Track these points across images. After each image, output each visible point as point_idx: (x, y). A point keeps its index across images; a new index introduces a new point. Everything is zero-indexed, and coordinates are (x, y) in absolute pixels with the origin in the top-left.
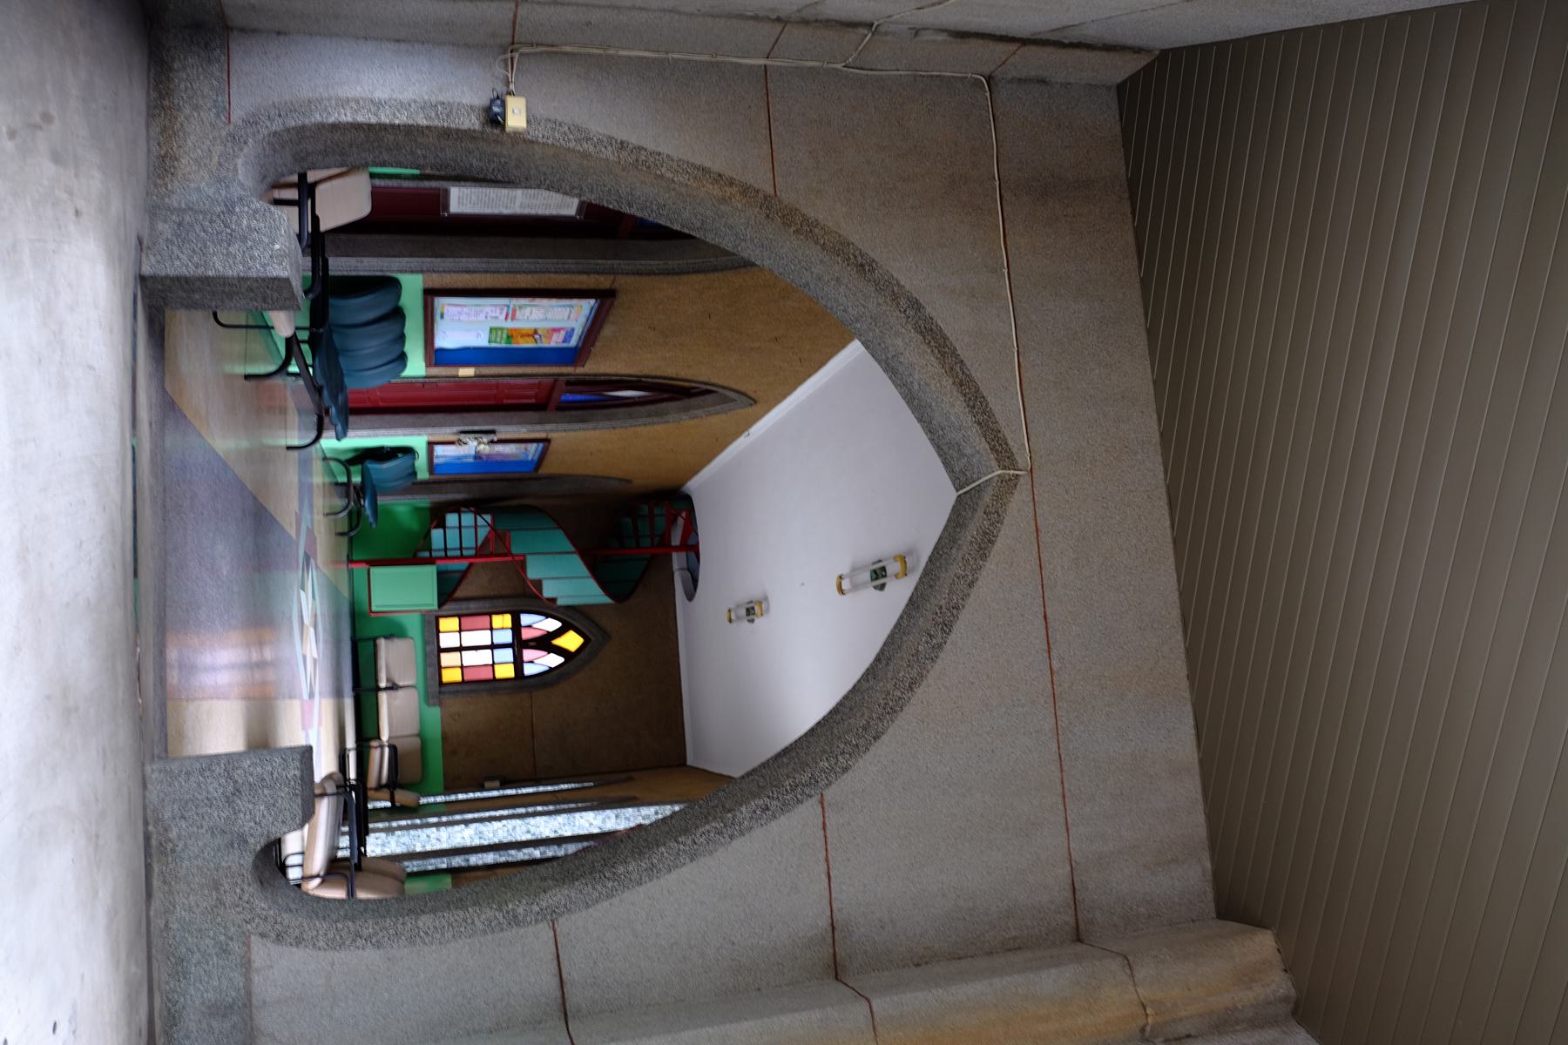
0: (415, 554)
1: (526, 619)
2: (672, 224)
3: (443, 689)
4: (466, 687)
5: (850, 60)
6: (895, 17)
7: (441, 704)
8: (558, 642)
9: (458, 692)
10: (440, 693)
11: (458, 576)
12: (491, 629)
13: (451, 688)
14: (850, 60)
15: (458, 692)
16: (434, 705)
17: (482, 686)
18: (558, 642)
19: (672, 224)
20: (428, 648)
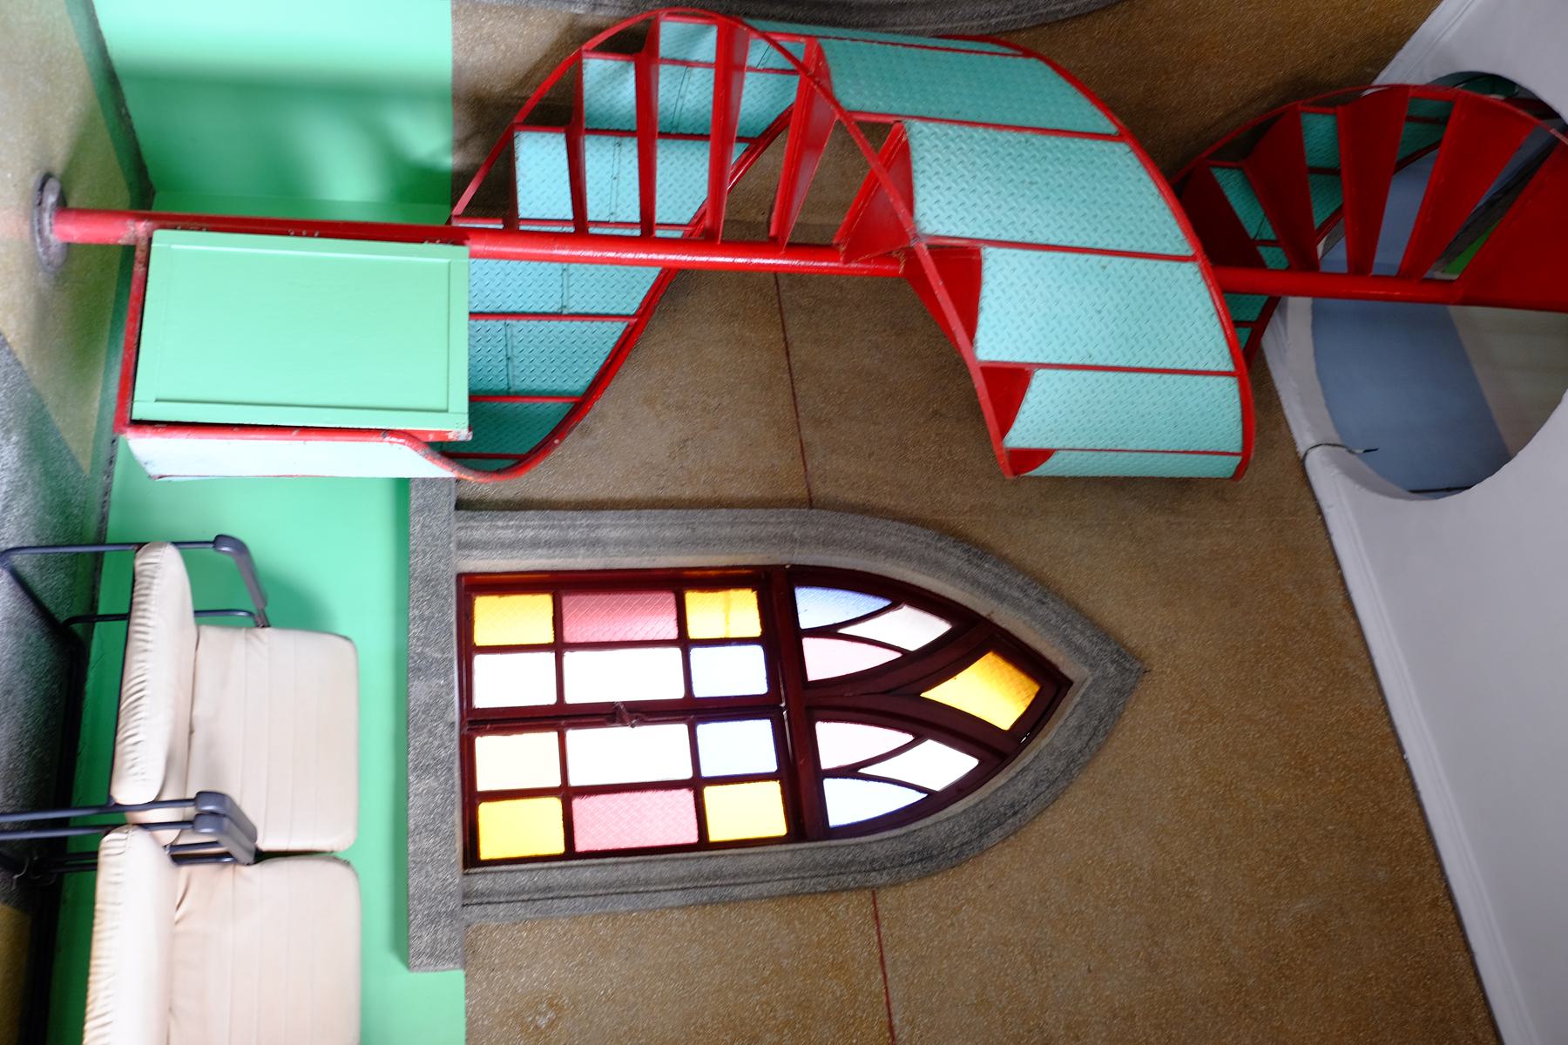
0: (449, 222)
1: (814, 607)
2: (661, 175)
3: (482, 882)
4: (587, 873)
5: (632, 522)
6: (604, 613)
7: (468, 956)
8: (947, 693)
9: (548, 893)
10: (469, 898)
11: (559, 409)
12: (684, 642)
13: (522, 878)
14: (632, 522)
15: (548, 893)
16: (436, 957)
17: (660, 868)
18: (947, 693)
19: (661, 175)
20: (420, 690)
